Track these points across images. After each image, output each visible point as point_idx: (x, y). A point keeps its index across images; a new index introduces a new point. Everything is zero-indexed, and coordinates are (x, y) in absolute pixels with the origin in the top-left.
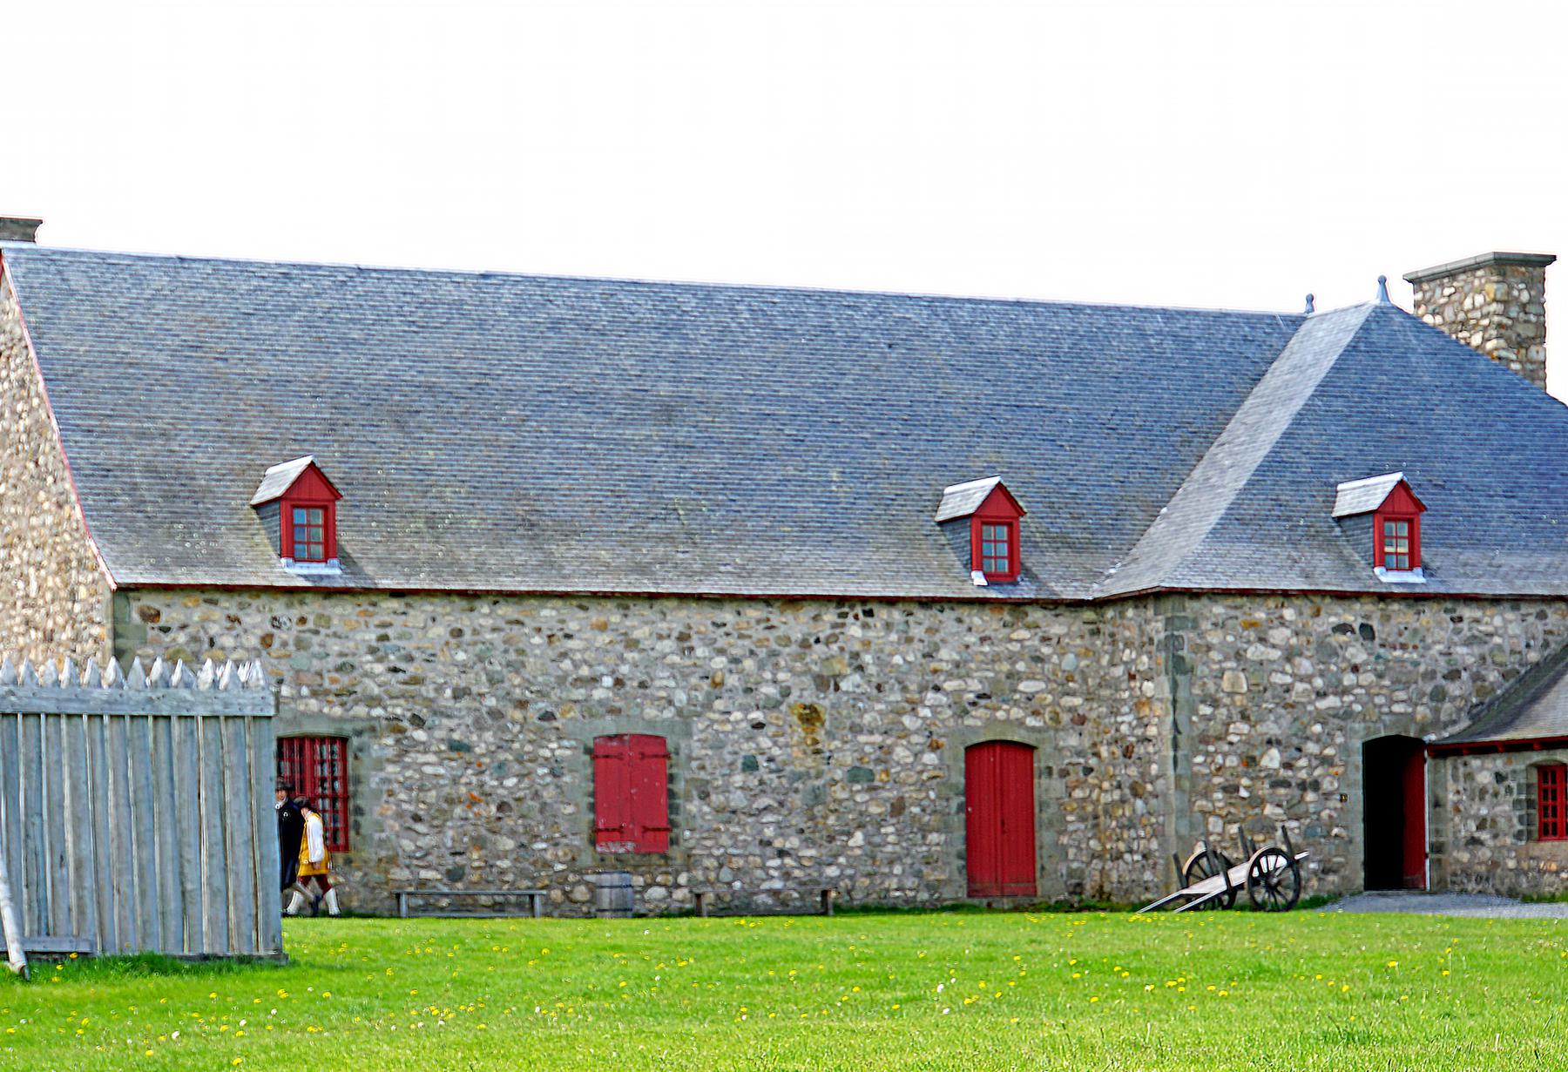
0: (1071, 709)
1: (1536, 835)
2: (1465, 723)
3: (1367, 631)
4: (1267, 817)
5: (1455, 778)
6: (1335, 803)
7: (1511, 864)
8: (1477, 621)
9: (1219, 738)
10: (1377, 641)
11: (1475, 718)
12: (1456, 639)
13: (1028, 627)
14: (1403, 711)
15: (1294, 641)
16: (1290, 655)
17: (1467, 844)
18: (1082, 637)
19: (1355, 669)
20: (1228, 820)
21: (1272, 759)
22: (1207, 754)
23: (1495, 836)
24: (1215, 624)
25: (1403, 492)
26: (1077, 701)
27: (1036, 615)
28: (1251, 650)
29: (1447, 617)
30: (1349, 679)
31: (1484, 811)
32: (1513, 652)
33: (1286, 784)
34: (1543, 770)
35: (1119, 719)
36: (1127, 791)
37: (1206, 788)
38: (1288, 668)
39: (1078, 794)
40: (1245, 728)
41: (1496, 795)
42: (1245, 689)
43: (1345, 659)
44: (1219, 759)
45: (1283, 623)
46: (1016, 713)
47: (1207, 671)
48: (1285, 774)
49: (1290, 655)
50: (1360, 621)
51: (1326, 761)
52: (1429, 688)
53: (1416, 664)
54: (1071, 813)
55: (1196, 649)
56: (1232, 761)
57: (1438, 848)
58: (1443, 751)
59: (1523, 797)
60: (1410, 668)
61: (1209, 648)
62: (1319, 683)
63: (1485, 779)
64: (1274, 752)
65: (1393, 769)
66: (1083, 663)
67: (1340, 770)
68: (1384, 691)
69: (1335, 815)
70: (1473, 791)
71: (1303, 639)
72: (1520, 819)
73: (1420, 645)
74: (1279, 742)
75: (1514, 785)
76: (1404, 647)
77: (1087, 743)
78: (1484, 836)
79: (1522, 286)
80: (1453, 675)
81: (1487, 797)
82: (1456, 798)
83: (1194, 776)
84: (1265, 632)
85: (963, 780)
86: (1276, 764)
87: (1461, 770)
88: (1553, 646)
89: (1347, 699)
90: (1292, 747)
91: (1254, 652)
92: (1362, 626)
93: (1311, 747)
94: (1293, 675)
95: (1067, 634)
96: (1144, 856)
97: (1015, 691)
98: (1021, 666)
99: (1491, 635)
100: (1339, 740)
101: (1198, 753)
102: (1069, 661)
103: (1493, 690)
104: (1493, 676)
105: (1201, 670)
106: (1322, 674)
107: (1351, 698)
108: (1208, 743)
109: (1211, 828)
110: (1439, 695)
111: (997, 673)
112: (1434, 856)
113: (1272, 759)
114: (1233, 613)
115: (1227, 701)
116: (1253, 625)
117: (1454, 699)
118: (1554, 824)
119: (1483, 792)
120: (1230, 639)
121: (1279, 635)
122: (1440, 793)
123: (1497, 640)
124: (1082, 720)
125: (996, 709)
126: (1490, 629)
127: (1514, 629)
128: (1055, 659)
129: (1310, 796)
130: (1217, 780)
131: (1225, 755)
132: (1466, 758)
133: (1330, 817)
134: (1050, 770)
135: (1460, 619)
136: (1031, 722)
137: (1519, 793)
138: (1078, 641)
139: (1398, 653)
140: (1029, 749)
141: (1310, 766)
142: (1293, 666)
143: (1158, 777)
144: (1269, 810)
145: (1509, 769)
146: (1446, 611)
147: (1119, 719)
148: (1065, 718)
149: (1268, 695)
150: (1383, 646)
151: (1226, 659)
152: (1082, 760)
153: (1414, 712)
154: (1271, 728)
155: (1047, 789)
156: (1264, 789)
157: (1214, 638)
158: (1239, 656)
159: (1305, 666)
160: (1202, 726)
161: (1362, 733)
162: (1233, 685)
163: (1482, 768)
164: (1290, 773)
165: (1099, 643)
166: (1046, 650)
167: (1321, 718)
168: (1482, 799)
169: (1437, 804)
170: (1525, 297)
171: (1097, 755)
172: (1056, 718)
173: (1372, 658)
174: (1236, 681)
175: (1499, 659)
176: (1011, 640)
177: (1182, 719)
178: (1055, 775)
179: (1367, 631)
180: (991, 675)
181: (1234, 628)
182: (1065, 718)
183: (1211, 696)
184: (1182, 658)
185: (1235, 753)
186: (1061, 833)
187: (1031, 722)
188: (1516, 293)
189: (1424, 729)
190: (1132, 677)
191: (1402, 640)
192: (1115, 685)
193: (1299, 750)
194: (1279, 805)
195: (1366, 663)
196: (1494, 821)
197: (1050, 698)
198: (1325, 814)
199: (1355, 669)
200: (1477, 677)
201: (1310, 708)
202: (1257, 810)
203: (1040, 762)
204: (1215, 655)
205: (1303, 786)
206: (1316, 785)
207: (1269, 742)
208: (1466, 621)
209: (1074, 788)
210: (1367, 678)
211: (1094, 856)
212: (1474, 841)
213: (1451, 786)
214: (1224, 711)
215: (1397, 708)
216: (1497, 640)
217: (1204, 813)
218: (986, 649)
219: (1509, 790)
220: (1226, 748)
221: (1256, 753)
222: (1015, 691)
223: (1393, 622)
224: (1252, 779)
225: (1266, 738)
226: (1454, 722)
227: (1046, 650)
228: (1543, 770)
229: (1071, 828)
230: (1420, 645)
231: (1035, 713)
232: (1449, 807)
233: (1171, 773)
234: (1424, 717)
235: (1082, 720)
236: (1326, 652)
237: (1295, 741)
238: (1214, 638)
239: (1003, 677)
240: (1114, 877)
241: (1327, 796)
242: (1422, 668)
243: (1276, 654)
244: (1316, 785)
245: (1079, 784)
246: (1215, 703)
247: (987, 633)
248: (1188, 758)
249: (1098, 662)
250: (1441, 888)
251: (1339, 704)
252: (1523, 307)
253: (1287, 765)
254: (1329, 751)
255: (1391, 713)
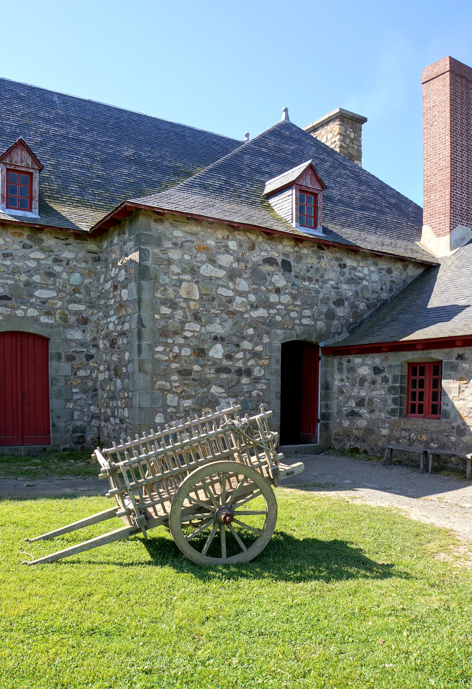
0: (76, 313)
1: (405, 412)
2: (345, 335)
3: (286, 266)
4: (212, 395)
6: (261, 386)
7: (385, 432)
8: (354, 269)
9: (176, 333)
10: (293, 273)
11: (352, 332)
13: (42, 250)
14: (305, 323)
15: (235, 265)
16: (233, 275)
18: (86, 262)
19: (278, 291)
20: (183, 396)
21: (217, 352)
23: (372, 411)
24: (175, 244)
26: (82, 307)
27: (49, 241)
28: (203, 267)
30: (273, 298)
31: (363, 394)
33: (227, 370)
37: (165, 371)
38: (231, 285)
39: (81, 373)
41: (374, 382)
42: (197, 297)
43: (271, 283)
44: (176, 349)
45: (227, 250)
46: (32, 312)
47: (167, 280)
48: (225, 363)
50: (282, 257)
52: (325, 310)
53: (318, 292)
54: (76, 387)
55: (158, 261)
56: (186, 352)
57: (326, 417)
60: (314, 295)
61: (170, 262)
62: (252, 298)
63: (364, 371)
64: (219, 347)
65: (300, 364)
66: (87, 281)
68: (297, 309)
69: (261, 394)
70: (355, 379)
71: (242, 265)
72: (395, 401)
75: (390, 376)
76: (310, 280)
77: (89, 337)
78: (363, 411)
79: (351, 130)
80: (339, 302)
81: (366, 384)
82: (340, 384)
83: (156, 362)
84: (214, 255)
87: (345, 364)
88: (395, 290)
89: (271, 311)
90: (231, 341)
91: (207, 270)
93: (246, 345)
94: (234, 290)
95: (75, 259)
97: (32, 296)
98: (37, 278)
99: (362, 279)
100: (266, 340)
102: (76, 278)
103: (362, 315)
104: (362, 306)
105: (164, 279)
106: (255, 292)
107: (275, 311)
108: (167, 336)
109: (168, 403)
110: (331, 316)
111: (16, 281)
112: (322, 422)
113: (217, 352)
114: (189, 238)
115: (183, 305)
116: (207, 249)
119: (362, 381)
120: (187, 257)
121: (226, 260)
122: (329, 379)
125: (14, 308)
126: (361, 275)
127: (375, 277)
128: (65, 275)
129: (245, 380)
130: (174, 366)
131: (181, 346)
132: (351, 357)
133: (258, 395)
135: (345, 266)
136: (44, 319)
138: (83, 265)
139: (306, 283)
140: (45, 340)
141: (244, 358)
142: (235, 284)
143: (129, 361)
144: (214, 389)
145: (386, 364)
146: (337, 259)
147: (109, 320)
148: (72, 319)
149: (216, 303)
150: (296, 277)
152: (85, 350)
153: (315, 324)
154: (216, 328)
155: (58, 369)
156: (210, 374)
157: (175, 255)
158: (193, 271)
159: (243, 285)
160: (163, 323)
161: (282, 337)
162: (188, 293)
163: (362, 365)
164: (231, 363)
165: (99, 267)
166: (58, 269)
167: (254, 323)
171: (96, 346)
172: (64, 318)
173: (290, 285)
174: (190, 290)
175: (366, 295)
176: (29, 259)
177: (145, 315)
179: (286, 266)
180: (10, 282)
182: (72, 319)
183: (170, 300)
184: (147, 268)
185: (189, 346)
186: (67, 401)
187: (44, 319)
189: (321, 336)
190: (115, 288)
191: (309, 274)
192: (103, 295)
193: (238, 346)
194: (221, 386)
195: (285, 287)
196: (371, 400)
197: (60, 304)
198: (254, 393)
199: (278, 291)
200: (353, 306)
202: (205, 389)
203: (52, 350)
205: (239, 372)
206: (248, 372)
207: (216, 338)
209: (79, 369)
210: (286, 299)
212: (353, 414)
213: (337, 376)
214: (180, 312)
215: (305, 321)
216: (365, 283)
218: (8, 263)
219: (385, 380)
220: (182, 341)
221: (206, 347)
223: (304, 261)
224: (202, 366)
225: (213, 335)
226: (339, 334)
227: (58, 269)
228: (414, 368)
229: (75, 397)
230: (320, 279)
231: (48, 314)
232: (335, 389)
233: (136, 358)
234: (321, 329)
235: (85, 321)
236: (258, 277)
237: (235, 339)
238: (175, 255)
239: (22, 284)
240: (105, 431)
241: (257, 380)
242: (321, 296)
243: (221, 273)
244: (248, 372)
245: (83, 367)
246: (174, 305)
247: (9, 251)
249: (98, 280)
250: (327, 449)
251: (266, 315)
252: (352, 140)
253: (229, 357)
254: (259, 348)
255: (301, 324)
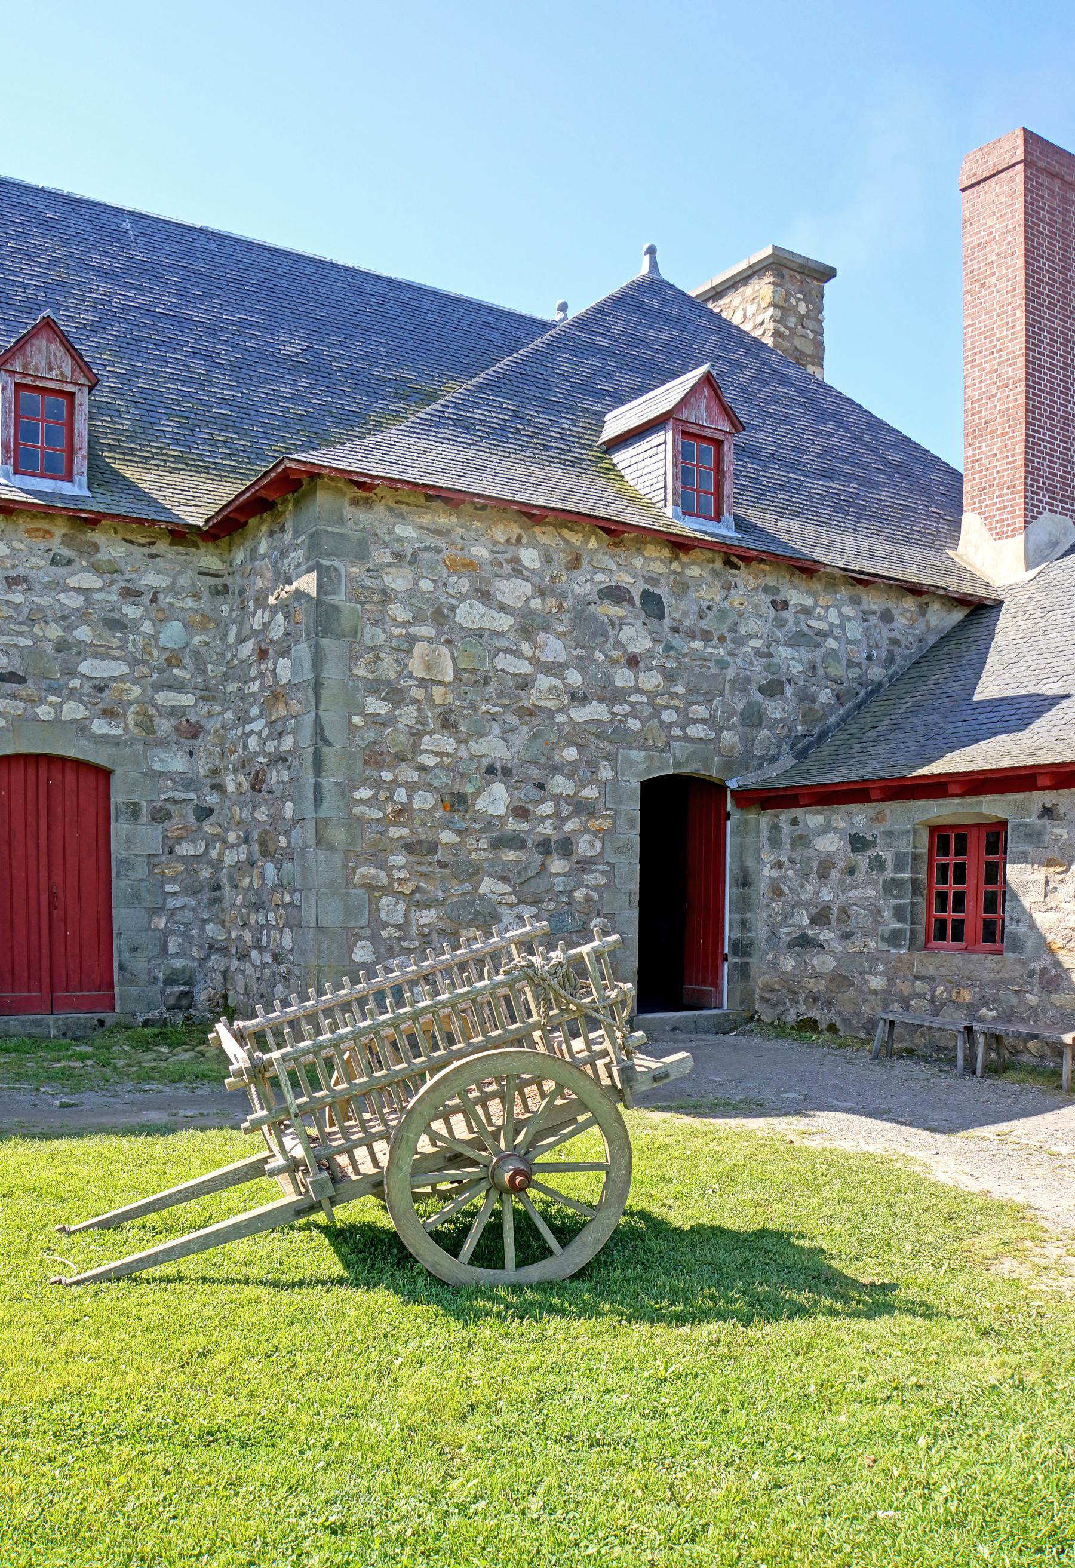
0: (173, 712)
1: (921, 937)
3: (652, 604)
4: (483, 898)
5: (775, 842)
7: (876, 983)
8: (807, 611)
10: (667, 622)
12: (778, 633)
13: (96, 569)
14: (694, 739)
15: (536, 603)
16: (530, 626)
17: (791, 945)
18: (196, 596)
19: (633, 662)
20: (416, 901)
21: (495, 800)
22: (378, 784)
23: (847, 936)
24: (398, 556)
25: (706, 391)
26: (186, 699)
27: (111, 547)
28: (463, 608)
29: (766, 599)
30: (623, 678)
31: (826, 896)
32: (851, 664)
33: (517, 842)
34: (942, 837)
35: (248, 728)
36: (256, 847)
37: (375, 843)
38: (526, 648)
39: (185, 849)
40: (449, 744)
41: (851, 871)
42: (449, 677)
43: (618, 644)
44: (401, 795)
45: (518, 570)
46: (73, 711)
47: (381, 638)
48: (514, 825)
49: (530, 626)
50: (642, 585)
51: (584, 808)
53: (723, 665)
54: (173, 880)
55: (360, 594)
56: (424, 800)
57: (741, 948)
58: (749, 798)
59: (906, 876)
60: (714, 670)
61: (387, 596)
62: (574, 677)
63: (830, 844)
64: (498, 788)
67: (606, 824)
68: (676, 702)
71: (552, 602)
72: (899, 913)
73: (730, 637)
74: (507, 772)
75: (888, 857)
76: (706, 636)
78: (826, 935)
79: (799, 296)
80: (772, 689)
81: (834, 874)
82: (774, 874)
84: (488, 582)
85: (1014, 873)
86: (500, 810)
89: (621, 709)
90: (528, 778)
91: (470, 614)
92: (646, 594)
93: (561, 785)
94: (533, 660)
95: (171, 589)
96: (276, 957)
97: (73, 674)
98: (83, 633)
99: (824, 635)
100: (606, 773)
101: (365, 782)
102: (173, 633)
103: (825, 717)
104: (825, 696)
105: (373, 635)
106: (581, 664)
107: (627, 708)
108: (380, 765)
109: (384, 916)
110: (753, 718)
111: (37, 640)
112: (733, 959)
114: (431, 541)
115: (417, 693)
117: (773, 725)
118: (958, 925)
119: (825, 866)
120: (426, 585)
121: (513, 591)
122: (750, 863)
123: (831, 643)
124: (195, 731)
125: (32, 701)
126: (823, 626)
127: (854, 630)
128: (147, 627)
129: (557, 865)
130: (395, 832)
131: (412, 788)
132: (798, 812)
133: (588, 899)
134: (134, 811)
136: (99, 727)
137: (899, 867)
138: (189, 603)
139: (698, 645)
141: (557, 814)
142: (535, 646)
144: (488, 886)
145: (878, 829)
146: (766, 590)
147: (248, 728)
148: (164, 726)
149: (491, 688)
150: (675, 630)
151: (418, 618)
152: (193, 796)
153: (718, 738)
154: (492, 747)
156: (479, 850)
157: (398, 580)
158: (441, 617)
160: (370, 735)
161: (642, 767)
162: (429, 667)
163: (825, 830)
164: (526, 826)
165: (225, 607)
166: (131, 611)
167: (577, 736)
168: (823, 876)
169: (744, 881)
170: (802, 308)
171: (219, 788)
172: (146, 724)
173: (659, 648)
174: (434, 660)
175: (833, 672)
176: (66, 589)
178: (144, 818)
179: (652, 604)
180: (23, 642)
181: (432, 568)
182: (164, 726)
183: (388, 683)
184: (336, 609)
186: (153, 912)
187: (99, 727)
188: (793, 301)
189: (729, 766)
191: (703, 625)
192: (235, 672)
193: (541, 787)
194: (504, 879)
195: (650, 654)
196: (844, 911)
197: (136, 691)
198: (579, 895)
199: (633, 662)
200: (805, 697)
201: (560, 718)
202: (467, 886)
204: (399, 611)
205: (545, 847)
207: (491, 770)
208: (792, 610)
209: (179, 840)
210: (651, 680)
211: (213, 948)
212: (804, 942)
213: (768, 856)
215: (693, 731)
216: (831, 643)
217: (370, 887)
218: (18, 598)
219: (878, 864)
220: (414, 776)
221: (469, 789)
222: (73, 674)
223: (692, 595)
224: (459, 832)
225: (485, 762)
226: (773, 759)
227: (131, 611)
228: (942, 837)
229: (171, 903)
230: (730, 637)
231: (108, 714)
233: (310, 814)
234: (732, 748)
235: (195, 731)
236: (587, 629)
237: (535, 772)
238: (398, 580)
239: (49, 647)
241: (585, 864)
242: (730, 673)
244: (566, 847)
246: (396, 695)
247: (21, 571)
248: (345, 790)
249: (224, 638)
251: (606, 717)
252: (801, 318)
253: (521, 812)
254: (590, 793)
255: (686, 738)
